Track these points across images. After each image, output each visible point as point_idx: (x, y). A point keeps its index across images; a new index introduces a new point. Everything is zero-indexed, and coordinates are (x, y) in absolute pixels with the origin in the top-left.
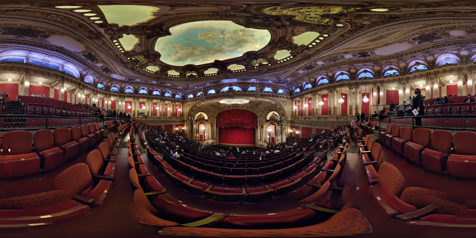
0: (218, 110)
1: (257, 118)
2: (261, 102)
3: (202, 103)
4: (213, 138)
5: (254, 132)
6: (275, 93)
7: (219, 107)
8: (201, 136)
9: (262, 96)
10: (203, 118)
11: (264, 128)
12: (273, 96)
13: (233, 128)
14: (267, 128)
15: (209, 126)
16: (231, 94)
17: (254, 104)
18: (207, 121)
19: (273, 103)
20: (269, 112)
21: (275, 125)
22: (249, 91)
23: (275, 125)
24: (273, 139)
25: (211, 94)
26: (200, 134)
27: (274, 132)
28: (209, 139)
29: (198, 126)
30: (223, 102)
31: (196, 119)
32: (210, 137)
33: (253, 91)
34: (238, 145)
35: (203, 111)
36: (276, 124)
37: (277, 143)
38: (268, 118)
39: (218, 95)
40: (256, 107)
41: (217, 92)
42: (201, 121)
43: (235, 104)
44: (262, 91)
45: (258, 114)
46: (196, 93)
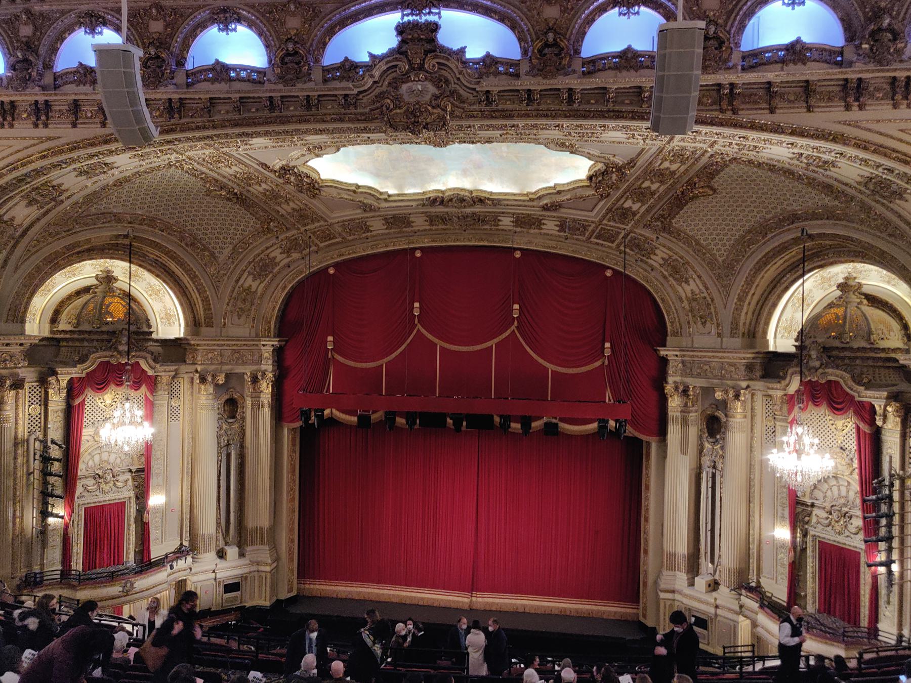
0: (293, 246)
1: (656, 330)
2: (707, 175)
3: (125, 162)
4: (238, 532)
5: (626, 465)
6: (877, 57)
7: (303, 216)
8: (102, 524)
9: (724, 105)
10: (136, 327)
11: (736, 439)
12: (854, 93)
13: (432, 421)
14: (772, 439)
15: (194, 412)
16: (418, 89)
17: (641, 195)
18: (175, 350)
19: (850, 168)
20: (799, 268)
21: (867, 413)
22: (595, 65)
23: (867, 413)
24: (839, 567)
25: (221, 71)
26: (89, 494)
27: (850, 486)
28: (190, 548)
29: (72, 417)
30: (347, 166)
31: (36, 325)
32: (208, 524)
33: (628, 59)
34: (484, 600)
35: (129, 251)
36: (877, 399)
37: (888, 630)
38: (780, 335)
39: (300, 90)
40: (664, 222)
41: (293, 55)
42: (110, 349)
43: (459, 199)
44: (719, 44)
45: (674, 297)
46: (40, 22)
